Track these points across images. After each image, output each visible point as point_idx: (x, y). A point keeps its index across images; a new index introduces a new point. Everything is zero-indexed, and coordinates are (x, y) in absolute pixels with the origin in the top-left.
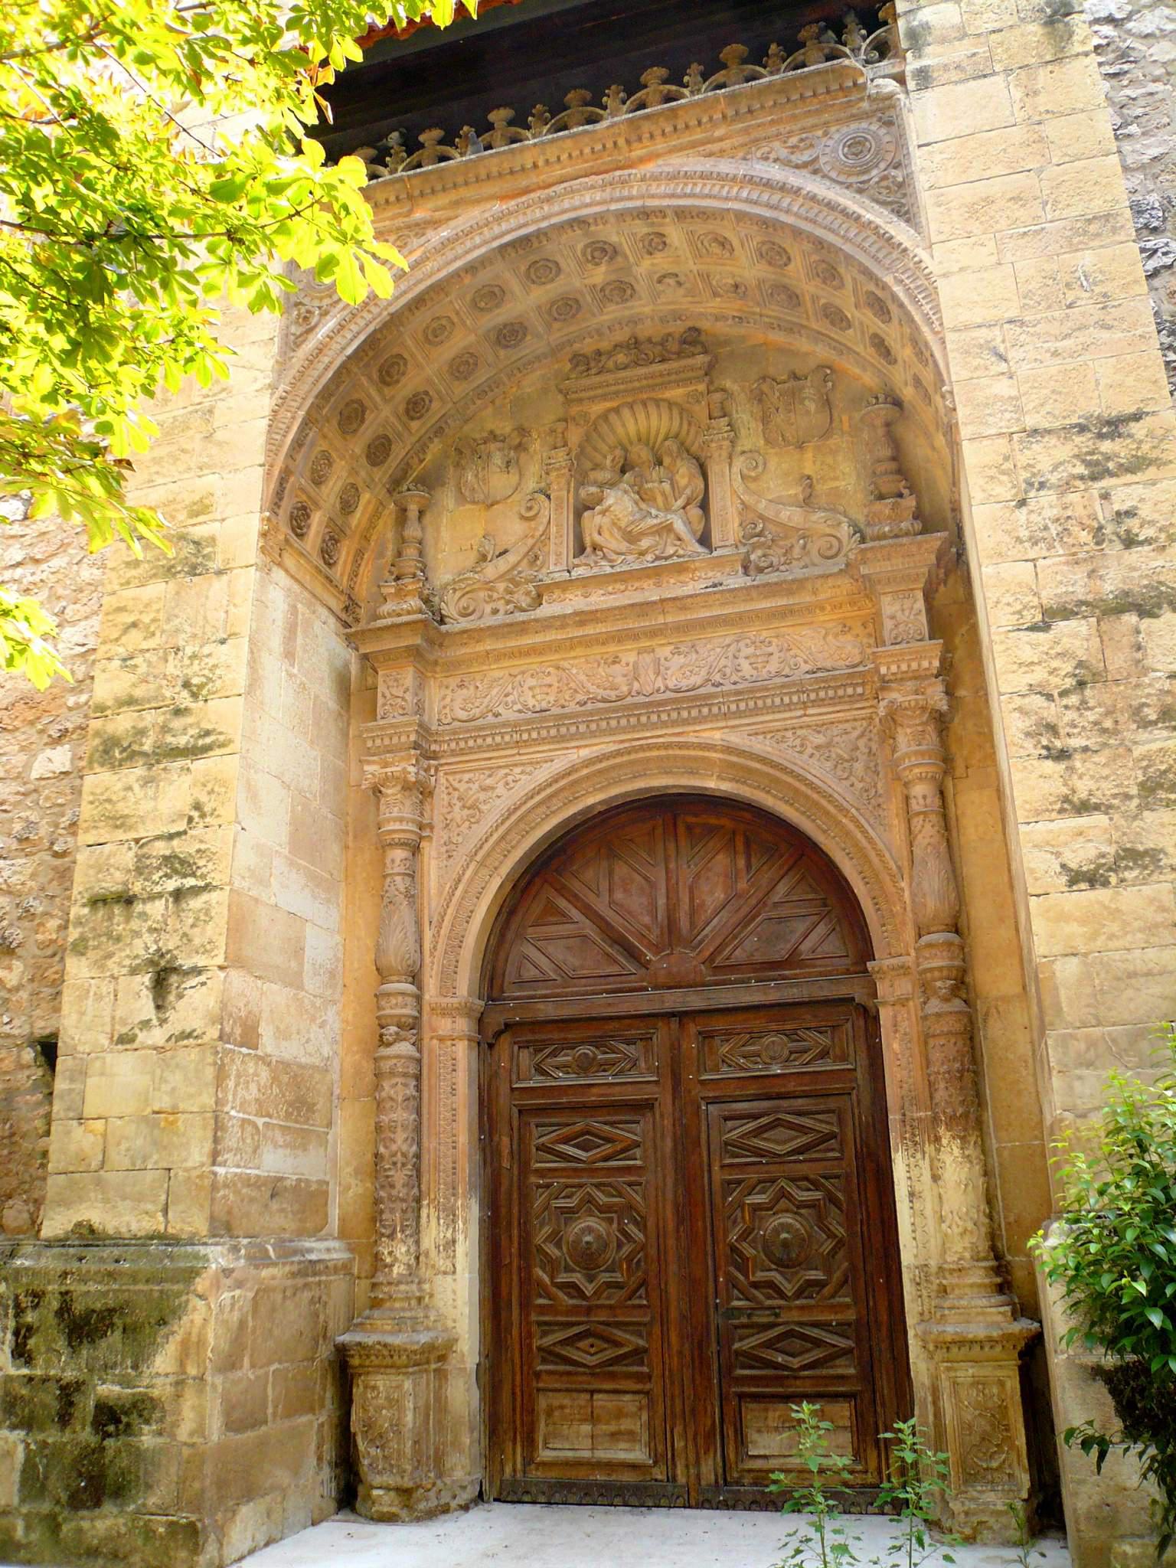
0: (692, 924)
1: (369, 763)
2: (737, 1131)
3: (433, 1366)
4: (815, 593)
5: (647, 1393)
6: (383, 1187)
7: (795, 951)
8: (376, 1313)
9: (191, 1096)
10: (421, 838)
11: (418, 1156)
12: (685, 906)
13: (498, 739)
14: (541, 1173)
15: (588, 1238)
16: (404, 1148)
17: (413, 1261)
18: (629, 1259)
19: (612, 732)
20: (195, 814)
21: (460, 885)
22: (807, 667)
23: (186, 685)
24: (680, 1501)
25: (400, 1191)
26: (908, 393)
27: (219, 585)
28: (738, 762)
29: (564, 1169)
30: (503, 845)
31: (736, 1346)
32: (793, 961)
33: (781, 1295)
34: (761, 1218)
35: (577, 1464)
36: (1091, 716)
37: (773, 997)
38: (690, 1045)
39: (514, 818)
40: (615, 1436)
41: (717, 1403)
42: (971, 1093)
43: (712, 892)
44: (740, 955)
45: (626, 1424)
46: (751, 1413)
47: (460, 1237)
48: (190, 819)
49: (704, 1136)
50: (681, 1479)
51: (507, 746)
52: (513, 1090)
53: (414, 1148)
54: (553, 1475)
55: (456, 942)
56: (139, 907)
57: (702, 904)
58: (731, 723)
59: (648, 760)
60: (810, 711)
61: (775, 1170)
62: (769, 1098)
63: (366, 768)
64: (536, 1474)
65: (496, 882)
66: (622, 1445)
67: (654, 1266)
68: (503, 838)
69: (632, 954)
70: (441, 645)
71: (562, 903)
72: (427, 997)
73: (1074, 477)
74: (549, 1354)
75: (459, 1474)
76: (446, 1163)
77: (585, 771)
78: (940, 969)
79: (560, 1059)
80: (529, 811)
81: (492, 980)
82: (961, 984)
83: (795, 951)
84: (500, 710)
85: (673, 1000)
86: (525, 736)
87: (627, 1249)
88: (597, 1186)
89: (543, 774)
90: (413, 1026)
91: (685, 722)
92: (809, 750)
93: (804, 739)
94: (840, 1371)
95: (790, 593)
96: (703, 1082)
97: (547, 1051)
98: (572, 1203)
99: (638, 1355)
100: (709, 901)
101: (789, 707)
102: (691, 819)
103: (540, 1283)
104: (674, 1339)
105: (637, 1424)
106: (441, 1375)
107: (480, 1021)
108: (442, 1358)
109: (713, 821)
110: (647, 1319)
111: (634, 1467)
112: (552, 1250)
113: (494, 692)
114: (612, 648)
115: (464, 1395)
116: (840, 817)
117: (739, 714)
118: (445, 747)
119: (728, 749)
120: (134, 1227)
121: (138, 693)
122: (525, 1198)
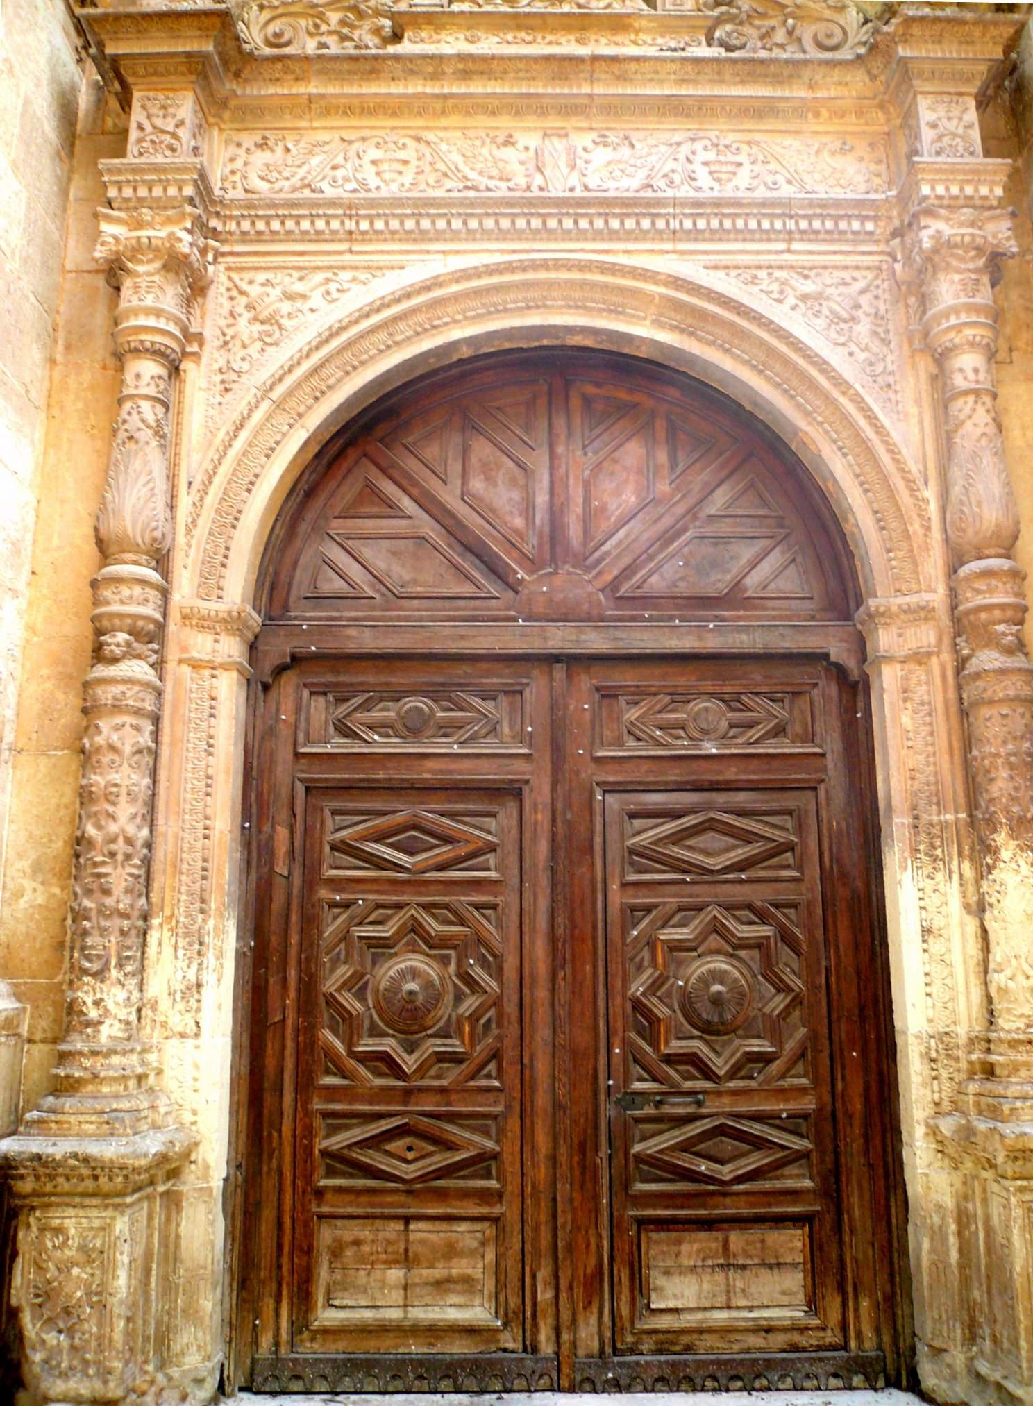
0: (586, 532)
1: (109, 219)
2: (649, 834)
3: (161, 1188)
4: (811, 87)
5: (495, 1220)
6: (89, 892)
7: (737, 585)
8: (68, 1103)
10: (185, 354)
11: (149, 845)
12: (576, 508)
13: (320, 224)
15: (412, 986)
16: (131, 830)
17: (133, 1017)
18: (474, 1018)
19: (502, 235)
24: (544, 1382)
25: (120, 899)
29: (374, 881)
30: (315, 381)
31: (637, 1148)
32: (734, 598)
33: (708, 1074)
34: (680, 963)
35: (383, 1329)
37: (712, 643)
38: (582, 704)
39: (335, 343)
40: (442, 1285)
41: (605, 1234)
43: (618, 492)
44: (656, 583)
45: (459, 1268)
46: (657, 1247)
47: (208, 978)
49: (598, 840)
50: (547, 1348)
51: (334, 237)
52: (298, 756)
53: (145, 832)
54: (336, 1349)
57: (603, 508)
58: (681, 246)
59: (551, 284)
60: (796, 246)
61: (703, 893)
62: (697, 788)
63: (104, 226)
64: (310, 1349)
65: (299, 437)
66: (454, 1299)
67: (514, 1030)
68: (315, 371)
69: (496, 570)
70: (237, 75)
71: (389, 488)
72: (176, 598)
74: (340, 1162)
75: (193, 1360)
76: (193, 861)
77: (455, 288)
78: (1002, 607)
79: (376, 715)
80: (362, 336)
81: (273, 588)
83: (737, 585)
84: (325, 185)
85: (559, 638)
86: (365, 225)
87: (470, 1003)
88: (427, 907)
90: (152, 635)
91: (613, 235)
92: (791, 300)
93: (784, 283)
94: (790, 1184)
95: (778, 80)
96: (598, 760)
97: (358, 700)
99: (482, 1163)
100: (612, 506)
101: (768, 236)
102: (590, 389)
103: (329, 1053)
104: (542, 1139)
105: (478, 1268)
106: (173, 1201)
107: (252, 647)
108: (174, 1174)
109: (623, 395)
110: (499, 1109)
111: (470, 1331)
112: (348, 1001)
113: (315, 161)
114: (505, 122)
115: (204, 1231)
116: (836, 394)
117: (695, 235)
118: (232, 226)
119: (676, 282)
122: (310, 922)
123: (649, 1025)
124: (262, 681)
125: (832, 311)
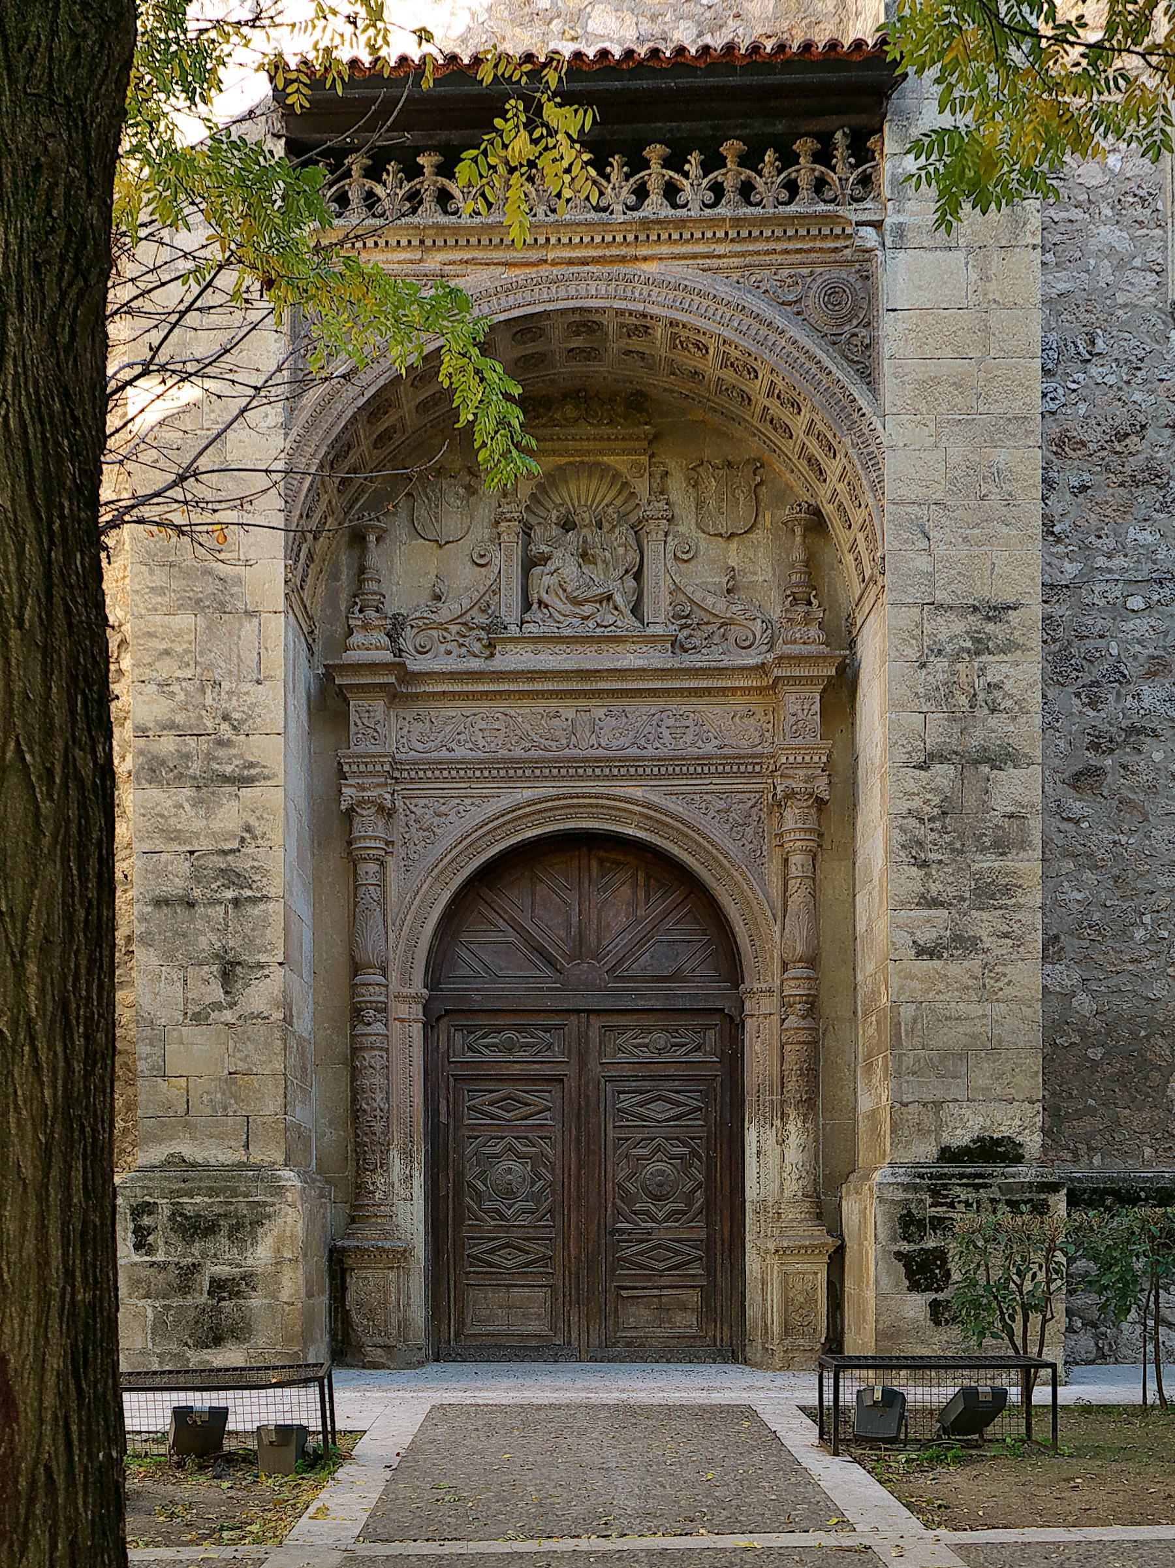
0: (599, 940)
9: (262, 1063)
14: (472, 1127)
20: (247, 835)
21: (412, 898)
22: (717, 743)
23: (226, 718)
26: (828, 509)
27: (249, 628)
28: (653, 815)
36: (947, 838)
42: (816, 1087)
43: (616, 916)
48: (243, 840)
55: (413, 943)
56: (200, 910)
69: (550, 962)
73: (963, 649)
82: (812, 1006)
84: (453, 745)
89: (493, 807)
92: (712, 813)
98: (498, 1150)
102: (602, 854)
103: (469, 1209)
109: (621, 858)
113: (448, 729)
114: (554, 703)
117: (659, 776)
120: (222, 1158)
121: (179, 718)
123: (629, 1199)
124: (430, 1025)
125: (734, 819)
